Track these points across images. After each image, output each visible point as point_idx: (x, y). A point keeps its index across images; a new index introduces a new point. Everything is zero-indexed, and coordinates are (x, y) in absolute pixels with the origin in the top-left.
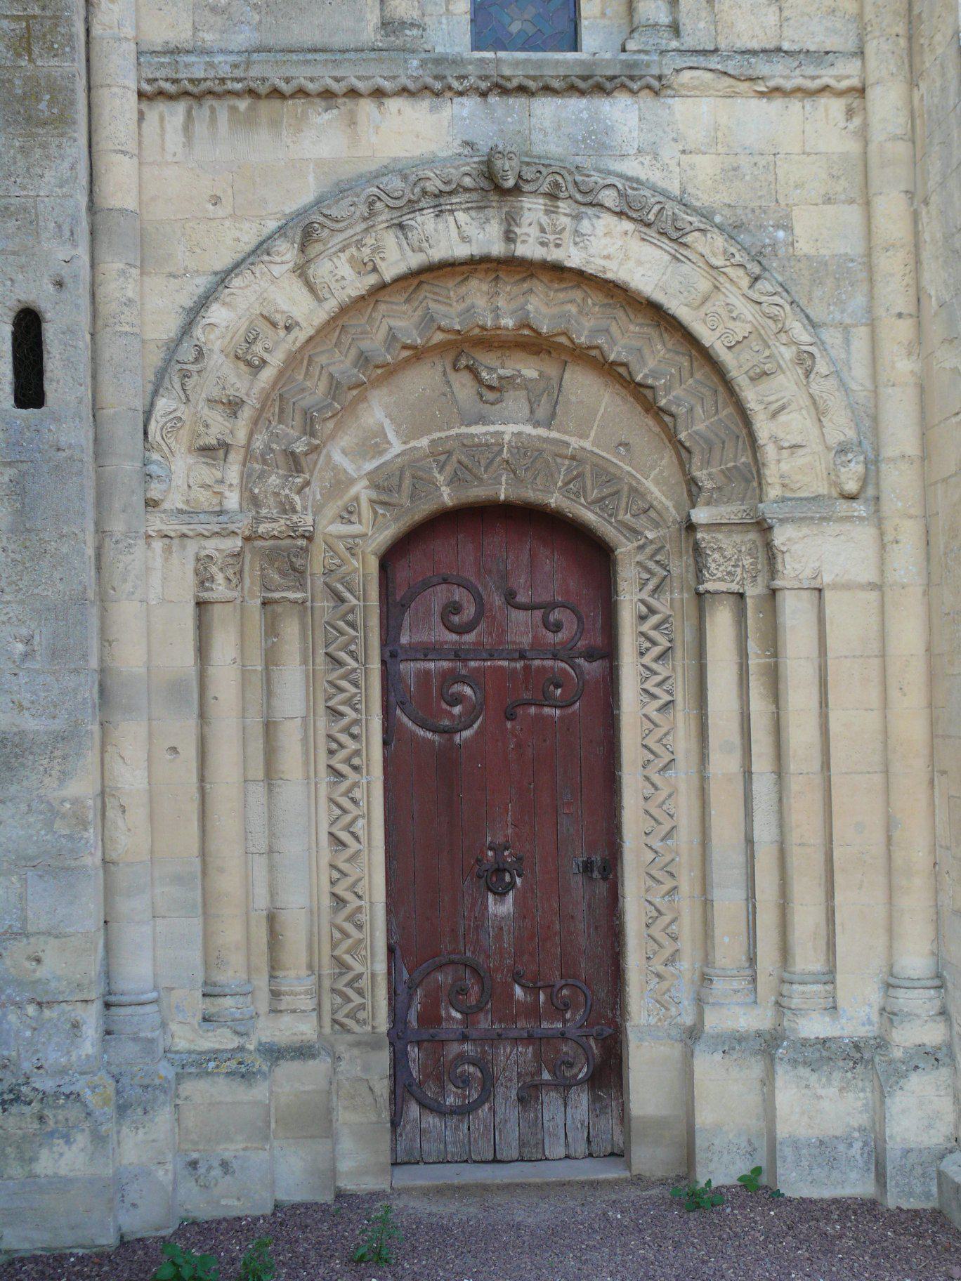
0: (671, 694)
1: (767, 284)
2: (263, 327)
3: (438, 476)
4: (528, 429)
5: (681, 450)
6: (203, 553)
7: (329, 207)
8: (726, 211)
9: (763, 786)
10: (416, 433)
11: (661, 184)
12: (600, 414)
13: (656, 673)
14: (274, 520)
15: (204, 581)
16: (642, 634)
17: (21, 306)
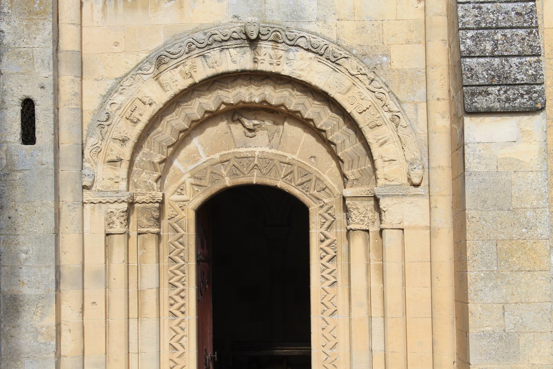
0: (335, 278)
1: (377, 83)
2: (138, 104)
3: (224, 172)
4: (267, 150)
5: (338, 160)
6: (109, 210)
7: (169, 48)
8: (359, 48)
9: (377, 323)
10: (213, 151)
11: (327, 35)
12: (302, 142)
13: (328, 268)
14: (144, 195)
15: (110, 224)
16: (321, 249)
17: (25, 98)
